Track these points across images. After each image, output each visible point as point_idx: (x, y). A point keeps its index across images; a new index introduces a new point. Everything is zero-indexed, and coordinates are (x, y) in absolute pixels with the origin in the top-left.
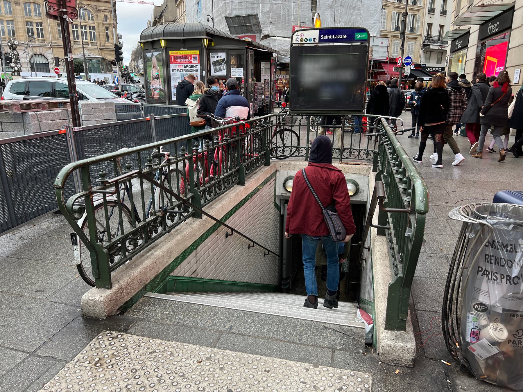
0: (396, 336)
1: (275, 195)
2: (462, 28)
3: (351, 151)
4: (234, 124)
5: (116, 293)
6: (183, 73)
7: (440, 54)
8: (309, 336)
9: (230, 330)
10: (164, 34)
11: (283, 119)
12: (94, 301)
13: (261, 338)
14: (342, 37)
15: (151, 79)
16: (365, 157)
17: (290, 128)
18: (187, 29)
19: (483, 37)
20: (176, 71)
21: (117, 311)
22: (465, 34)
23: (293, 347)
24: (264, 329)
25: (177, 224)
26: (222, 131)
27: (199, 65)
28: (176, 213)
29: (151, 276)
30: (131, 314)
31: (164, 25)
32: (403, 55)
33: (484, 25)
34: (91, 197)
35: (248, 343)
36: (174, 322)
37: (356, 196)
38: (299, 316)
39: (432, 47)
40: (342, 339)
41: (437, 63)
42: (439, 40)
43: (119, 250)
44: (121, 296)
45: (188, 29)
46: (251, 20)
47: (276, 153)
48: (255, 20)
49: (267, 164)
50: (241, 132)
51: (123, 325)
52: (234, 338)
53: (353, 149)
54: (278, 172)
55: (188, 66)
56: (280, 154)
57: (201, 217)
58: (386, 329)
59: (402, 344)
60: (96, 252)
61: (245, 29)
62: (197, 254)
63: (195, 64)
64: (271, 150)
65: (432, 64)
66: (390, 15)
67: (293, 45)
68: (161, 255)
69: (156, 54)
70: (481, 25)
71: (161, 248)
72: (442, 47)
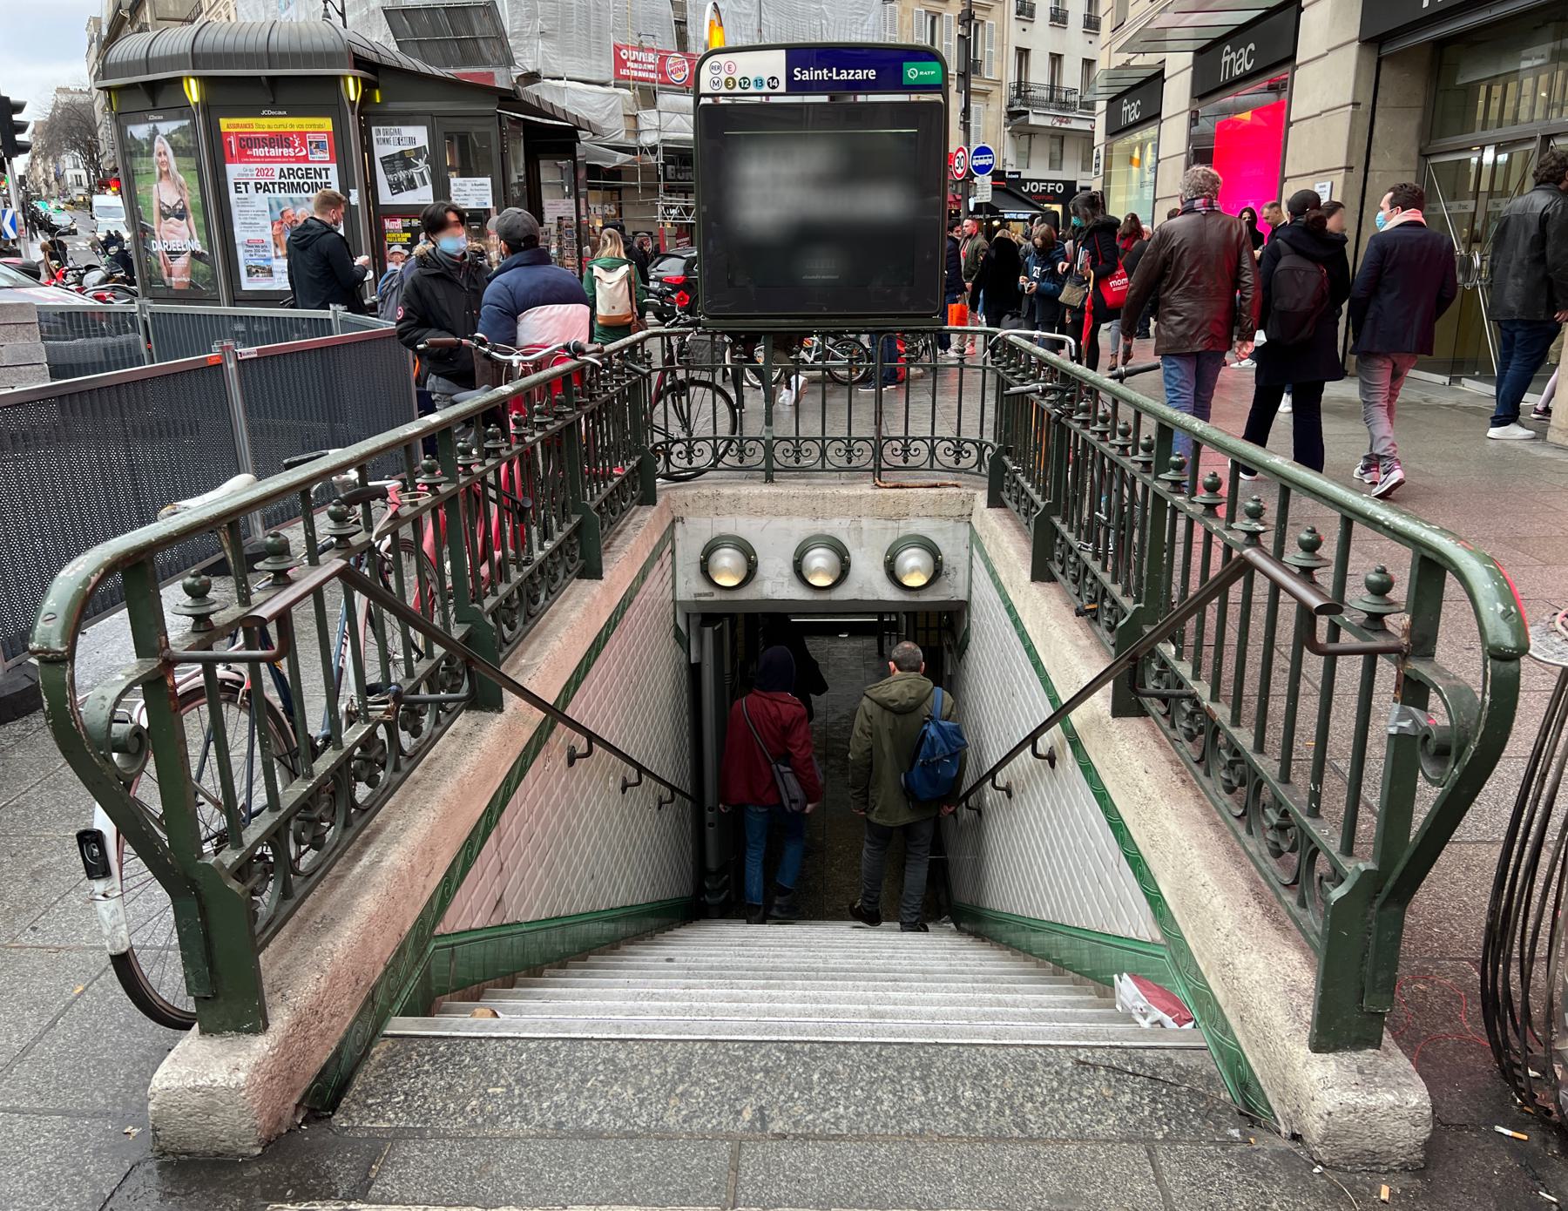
0: (1360, 1071)
1: (674, 601)
2: (1140, 60)
3: (906, 445)
4: (559, 368)
5: (286, 1043)
6: (277, 195)
7: (1057, 141)
8: (1044, 1104)
9: (764, 1127)
10: (197, 58)
11: (681, 346)
12: (209, 1092)
13: (886, 1139)
14: (860, 75)
15: (155, 222)
16: (950, 461)
17: (705, 376)
18: (280, 40)
19: (1206, 87)
20: (251, 187)
21: (296, 1114)
22: (1148, 80)
23: (1012, 1156)
24: (880, 1101)
25: (433, 740)
26: (522, 398)
27: (333, 167)
28: (425, 702)
29: (382, 953)
30: (362, 1119)
31: (152, 34)
32: (967, 143)
33: (1207, 53)
34: (170, 682)
35: (850, 1166)
36: (543, 1126)
37: (931, 588)
38: (978, 1034)
39: (1033, 120)
40: (1154, 1101)
41: (1051, 167)
42: (1051, 99)
43: (268, 869)
44: (302, 1053)
45: (284, 40)
46: (475, 23)
47: (668, 461)
48: (487, 20)
49: (649, 498)
50: (577, 394)
51: (344, 1172)
52: (790, 1155)
53: (915, 439)
54: (679, 525)
55: (291, 172)
56: (679, 463)
57: (497, 706)
58: (1317, 1047)
59: (1391, 1098)
60: (199, 897)
61: (454, 51)
62: (499, 841)
63: (318, 166)
64: (654, 450)
65: (1038, 171)
66: (907, 18)
67: (703, 101)
68: (405, 866)
69: (167, 127)
70: (1199, 53)
71: (395, 840)
72: (1061, 119)
